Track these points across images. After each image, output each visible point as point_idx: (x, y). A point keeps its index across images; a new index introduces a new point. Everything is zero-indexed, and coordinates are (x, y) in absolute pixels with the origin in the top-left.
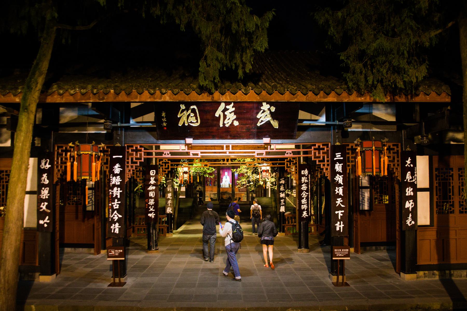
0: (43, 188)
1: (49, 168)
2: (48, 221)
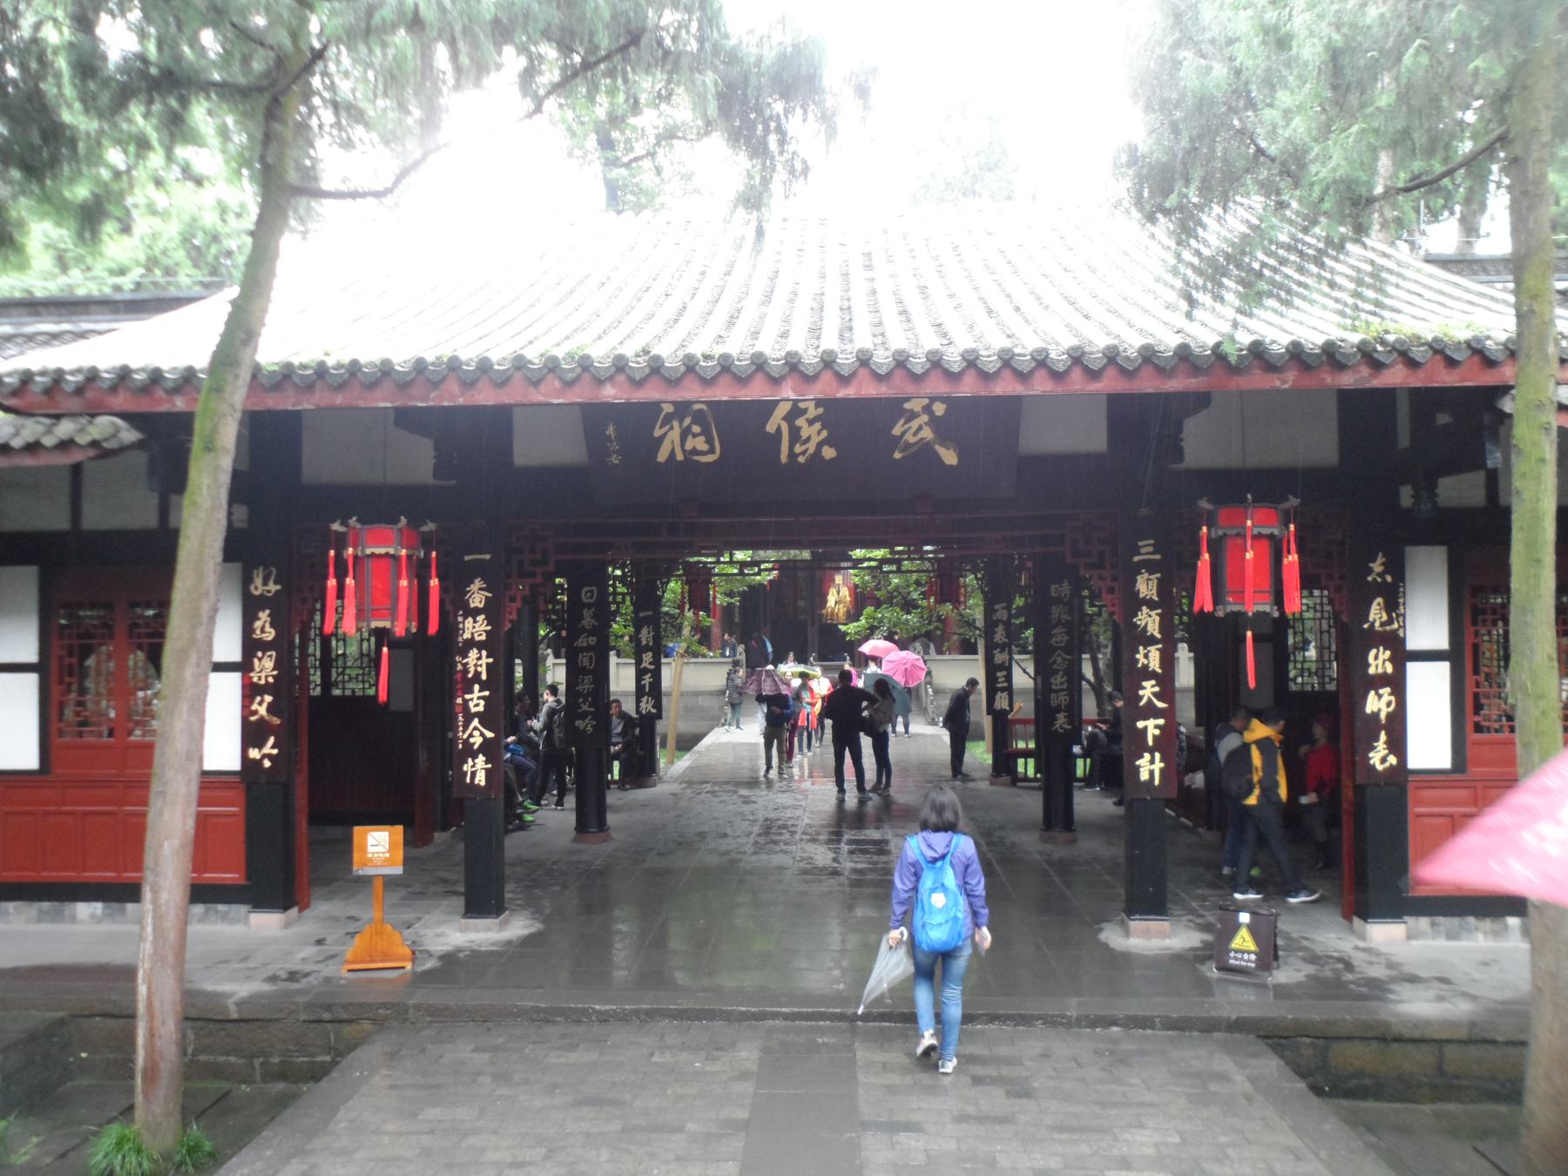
0: (260, 654)
1: (277, 592)
2: (275, 751)
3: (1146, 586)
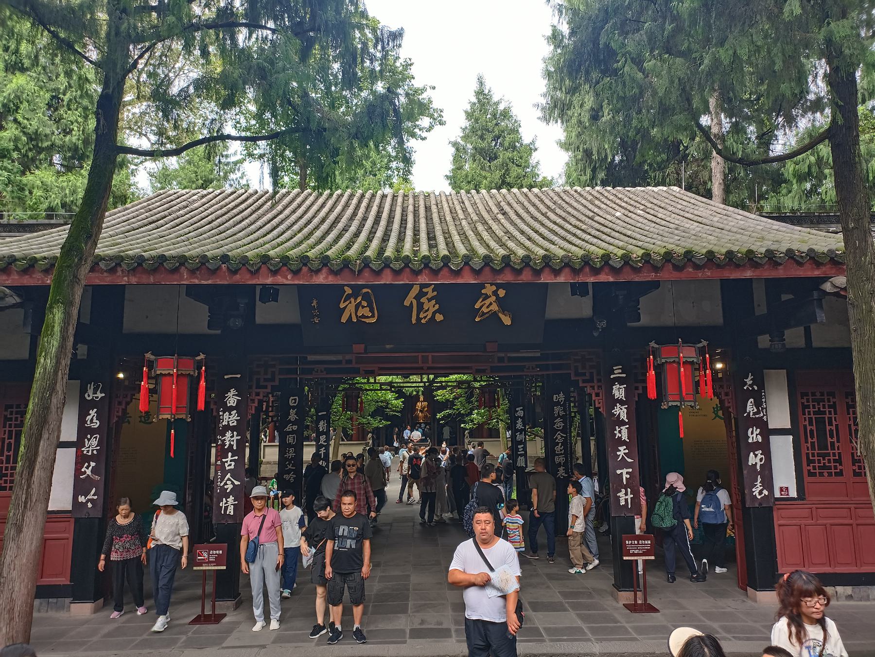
3: (619, 392)
